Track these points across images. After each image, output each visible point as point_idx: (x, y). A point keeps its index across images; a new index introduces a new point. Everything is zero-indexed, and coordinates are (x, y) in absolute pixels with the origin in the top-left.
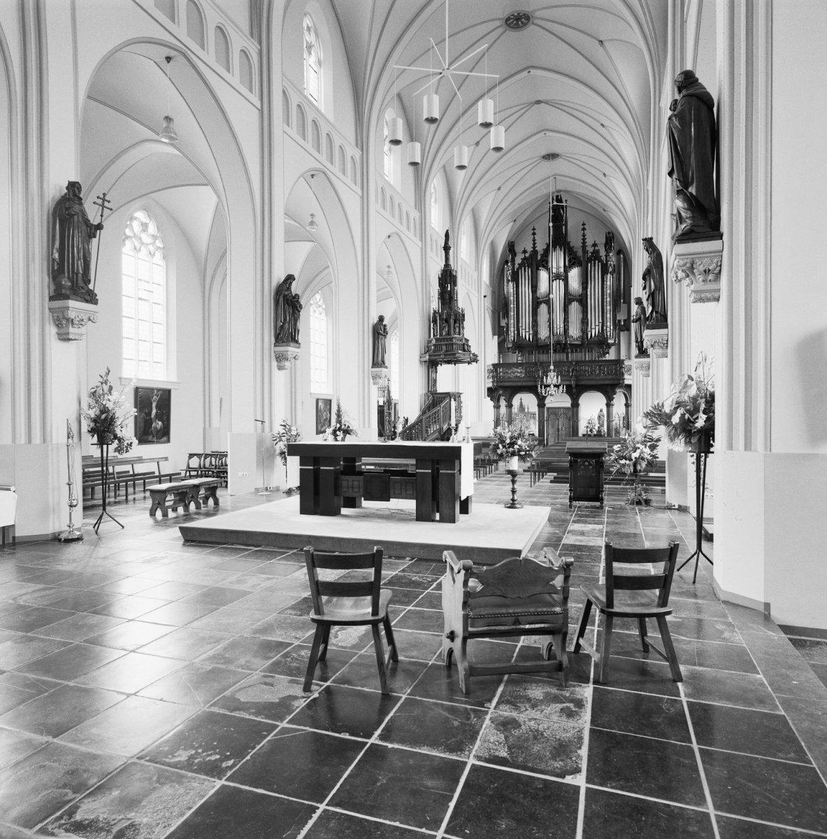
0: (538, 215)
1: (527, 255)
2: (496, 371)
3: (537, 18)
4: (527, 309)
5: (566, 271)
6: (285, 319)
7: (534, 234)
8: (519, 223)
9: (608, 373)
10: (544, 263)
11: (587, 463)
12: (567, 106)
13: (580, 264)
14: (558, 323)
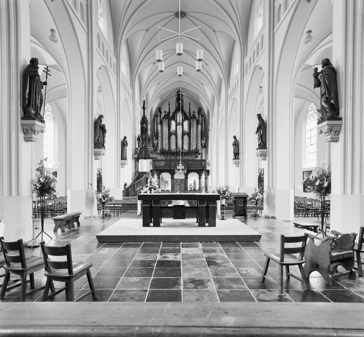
0: (170, 97)
1: (166, 113)
2: (154, 163)
3: (189, 15)
4: (166, 136)
5: (183, 122)
6: (100, 136)
7: (190, 105)
8: (163, 99)
9: (200, 165)
10: (174, 118)
11: (240, 201)
12: (190, 53)
13: (188, 119)
14: (179, 143)
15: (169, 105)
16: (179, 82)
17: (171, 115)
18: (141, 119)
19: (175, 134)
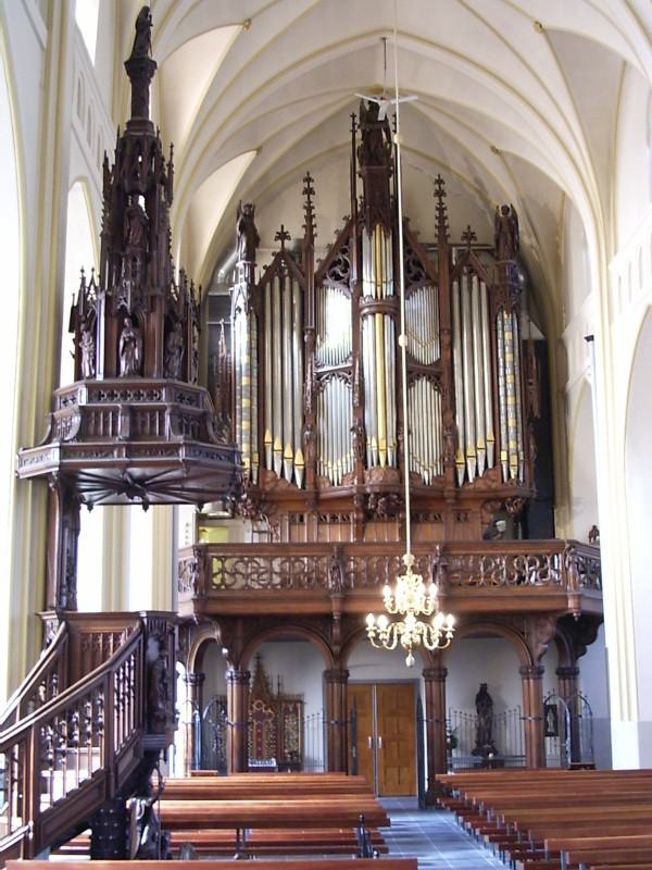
15: (309, 191)
16: (375, 39)
17: (320, 254)
18: (111, 146)
19: (349, 371)
